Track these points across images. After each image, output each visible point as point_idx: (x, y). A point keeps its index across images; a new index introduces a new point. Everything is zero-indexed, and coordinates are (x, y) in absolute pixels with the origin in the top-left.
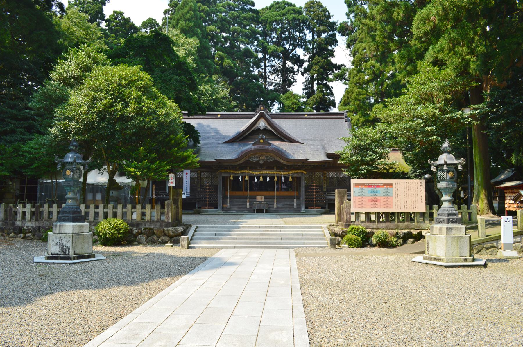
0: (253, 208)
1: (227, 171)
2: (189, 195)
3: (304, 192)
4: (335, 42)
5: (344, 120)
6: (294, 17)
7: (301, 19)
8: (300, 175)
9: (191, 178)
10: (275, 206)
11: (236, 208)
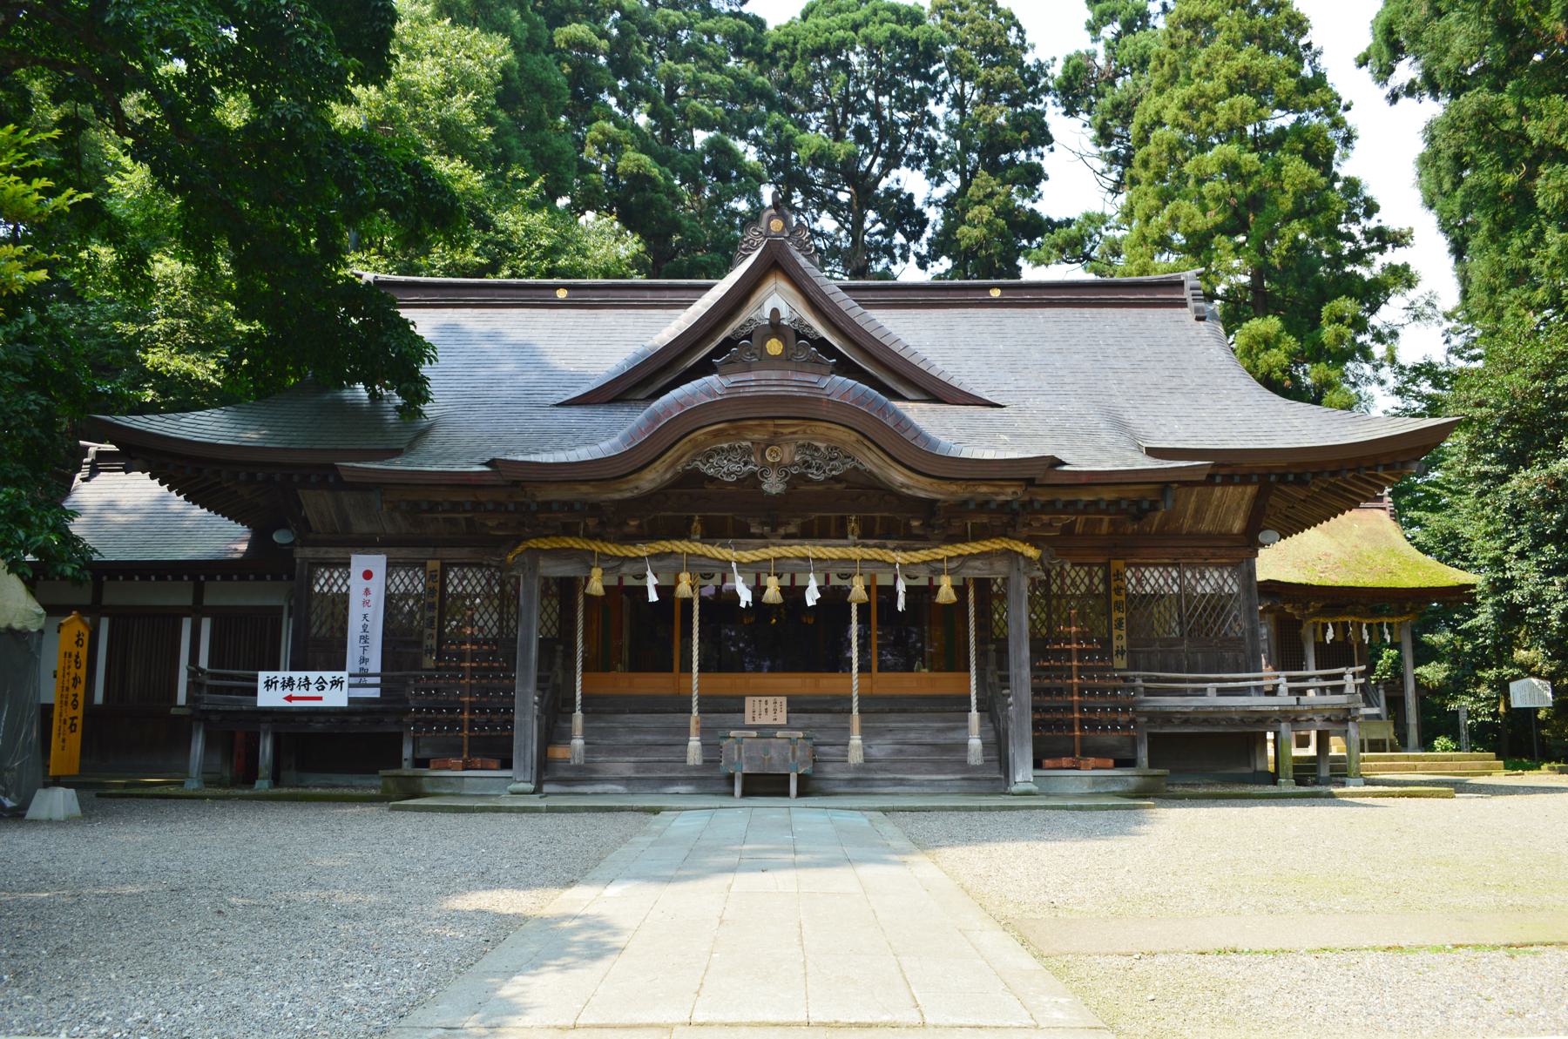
0: (724, 768)
1: (571, 542)
2: (375, 693)
3: (1026, 672)
5: (1187, 315)
6: (893, 34)
7: (922, 39)
8: (1000, 569)
9: (389, 598)
10: (855, 756)
11: (624, 766)
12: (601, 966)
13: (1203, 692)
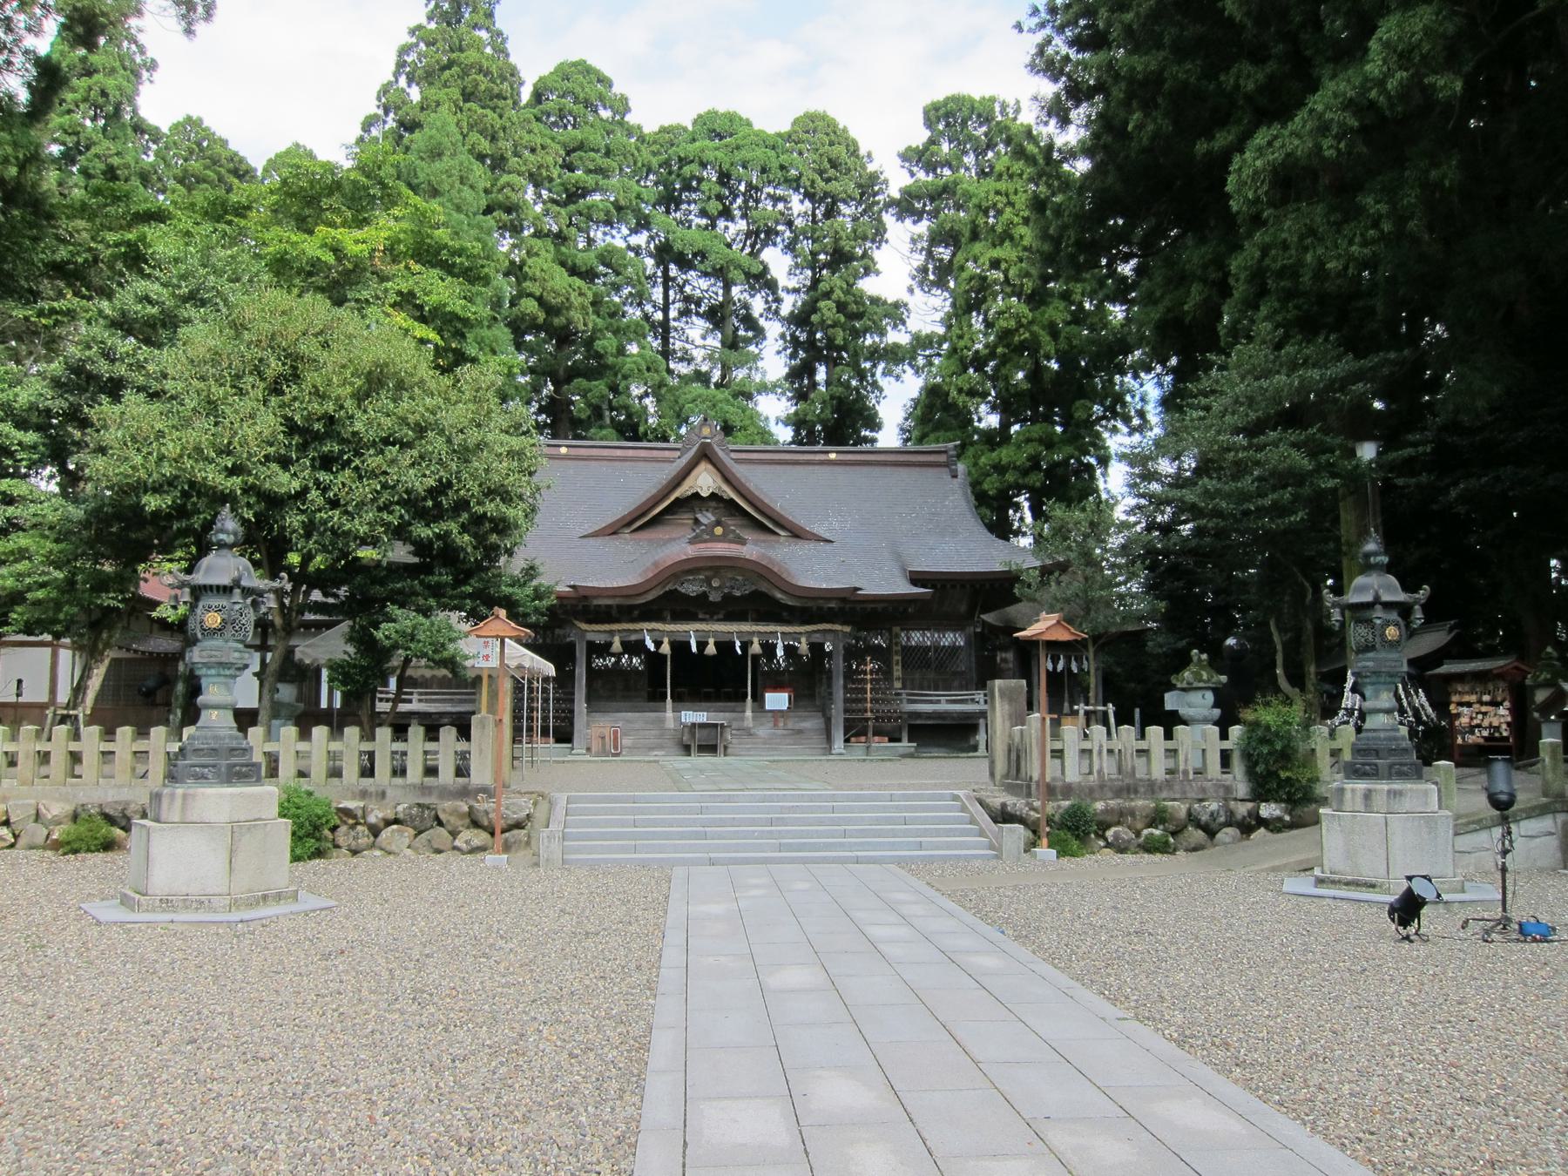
3: (841, 692)
4: (879, 235)
12: (110, 855)
13: (938, 702)
